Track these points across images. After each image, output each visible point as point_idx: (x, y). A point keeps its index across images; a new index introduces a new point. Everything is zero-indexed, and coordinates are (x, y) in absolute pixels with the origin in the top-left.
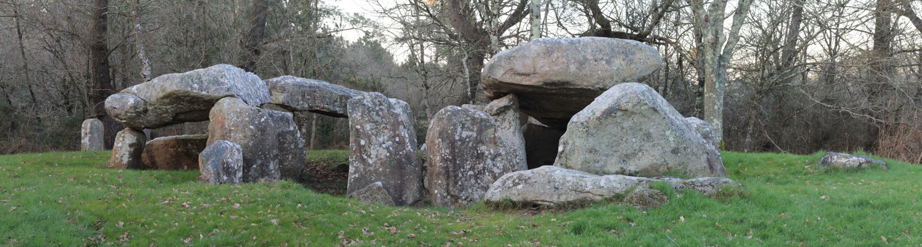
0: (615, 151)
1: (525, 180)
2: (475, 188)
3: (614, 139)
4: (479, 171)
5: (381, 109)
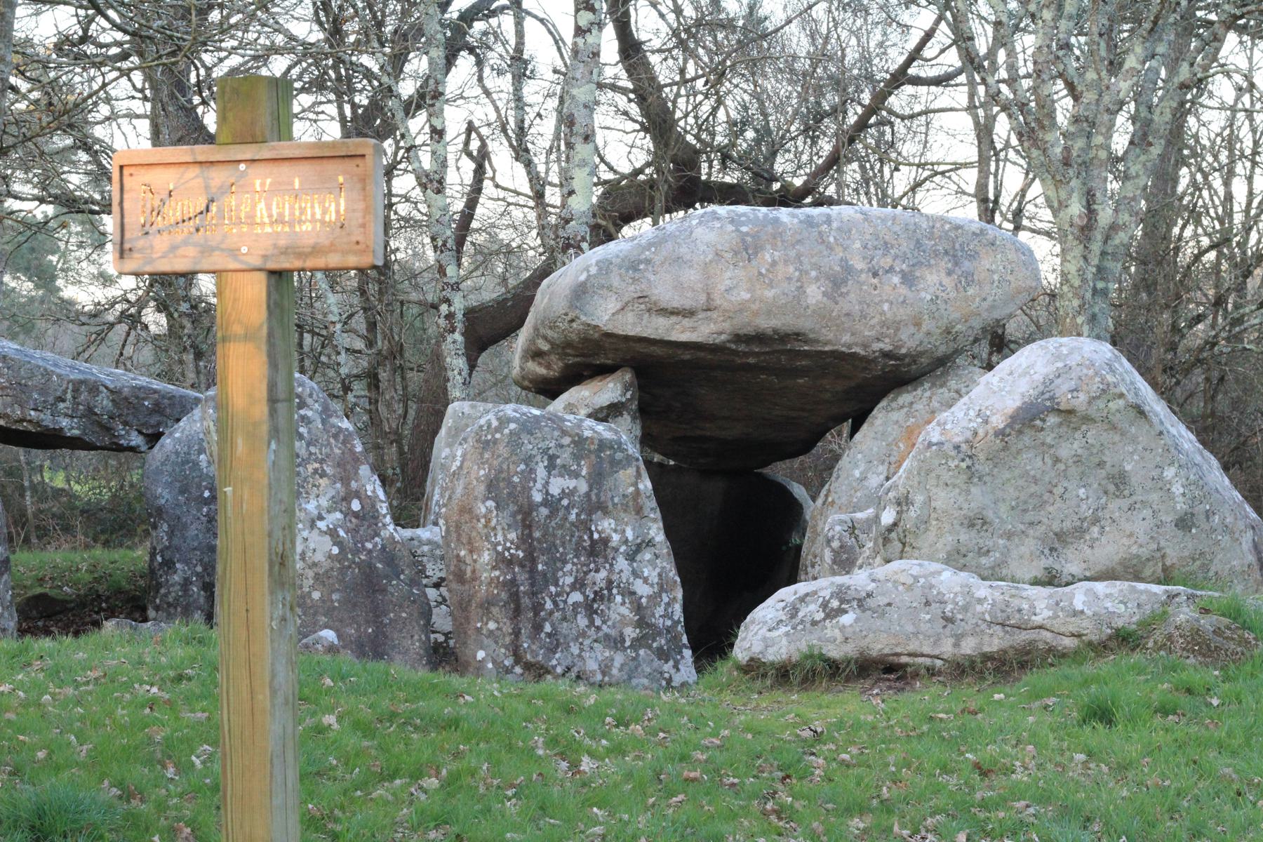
0: (1031, 524)
1: (859, 600)
2: (587, 642)
3: (1033, 488)
4: (596, 593)
5: (303, 418)
